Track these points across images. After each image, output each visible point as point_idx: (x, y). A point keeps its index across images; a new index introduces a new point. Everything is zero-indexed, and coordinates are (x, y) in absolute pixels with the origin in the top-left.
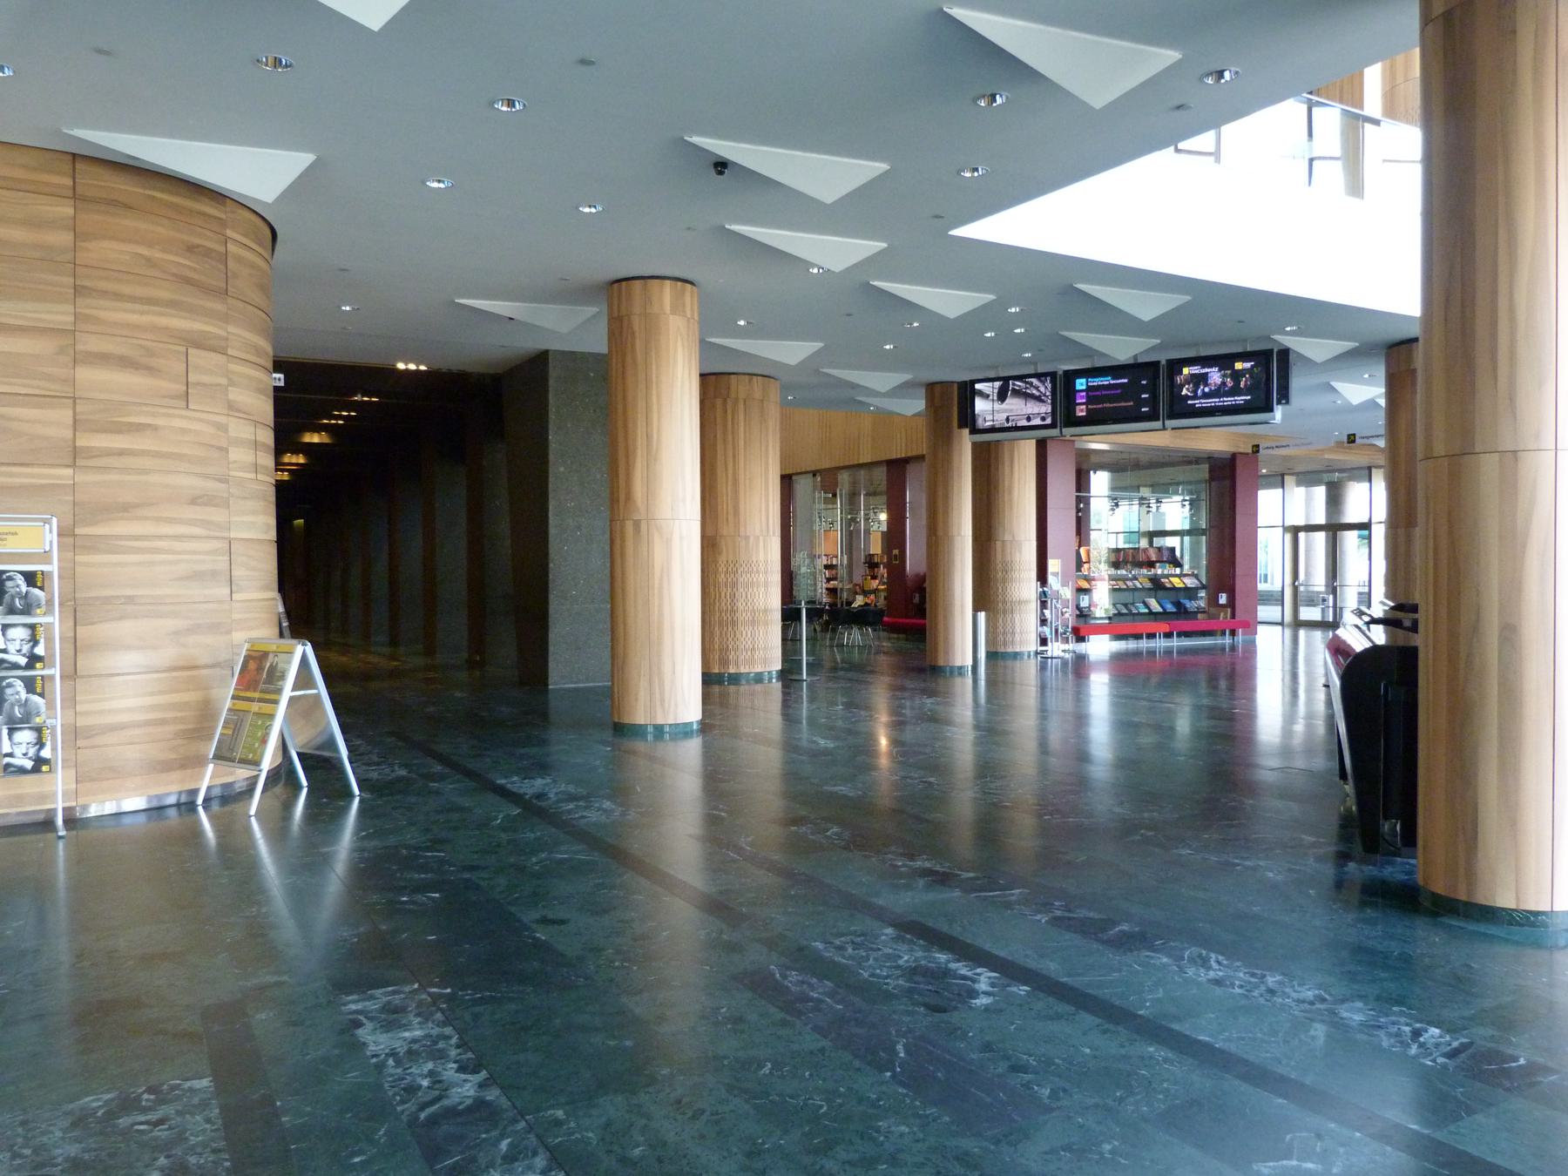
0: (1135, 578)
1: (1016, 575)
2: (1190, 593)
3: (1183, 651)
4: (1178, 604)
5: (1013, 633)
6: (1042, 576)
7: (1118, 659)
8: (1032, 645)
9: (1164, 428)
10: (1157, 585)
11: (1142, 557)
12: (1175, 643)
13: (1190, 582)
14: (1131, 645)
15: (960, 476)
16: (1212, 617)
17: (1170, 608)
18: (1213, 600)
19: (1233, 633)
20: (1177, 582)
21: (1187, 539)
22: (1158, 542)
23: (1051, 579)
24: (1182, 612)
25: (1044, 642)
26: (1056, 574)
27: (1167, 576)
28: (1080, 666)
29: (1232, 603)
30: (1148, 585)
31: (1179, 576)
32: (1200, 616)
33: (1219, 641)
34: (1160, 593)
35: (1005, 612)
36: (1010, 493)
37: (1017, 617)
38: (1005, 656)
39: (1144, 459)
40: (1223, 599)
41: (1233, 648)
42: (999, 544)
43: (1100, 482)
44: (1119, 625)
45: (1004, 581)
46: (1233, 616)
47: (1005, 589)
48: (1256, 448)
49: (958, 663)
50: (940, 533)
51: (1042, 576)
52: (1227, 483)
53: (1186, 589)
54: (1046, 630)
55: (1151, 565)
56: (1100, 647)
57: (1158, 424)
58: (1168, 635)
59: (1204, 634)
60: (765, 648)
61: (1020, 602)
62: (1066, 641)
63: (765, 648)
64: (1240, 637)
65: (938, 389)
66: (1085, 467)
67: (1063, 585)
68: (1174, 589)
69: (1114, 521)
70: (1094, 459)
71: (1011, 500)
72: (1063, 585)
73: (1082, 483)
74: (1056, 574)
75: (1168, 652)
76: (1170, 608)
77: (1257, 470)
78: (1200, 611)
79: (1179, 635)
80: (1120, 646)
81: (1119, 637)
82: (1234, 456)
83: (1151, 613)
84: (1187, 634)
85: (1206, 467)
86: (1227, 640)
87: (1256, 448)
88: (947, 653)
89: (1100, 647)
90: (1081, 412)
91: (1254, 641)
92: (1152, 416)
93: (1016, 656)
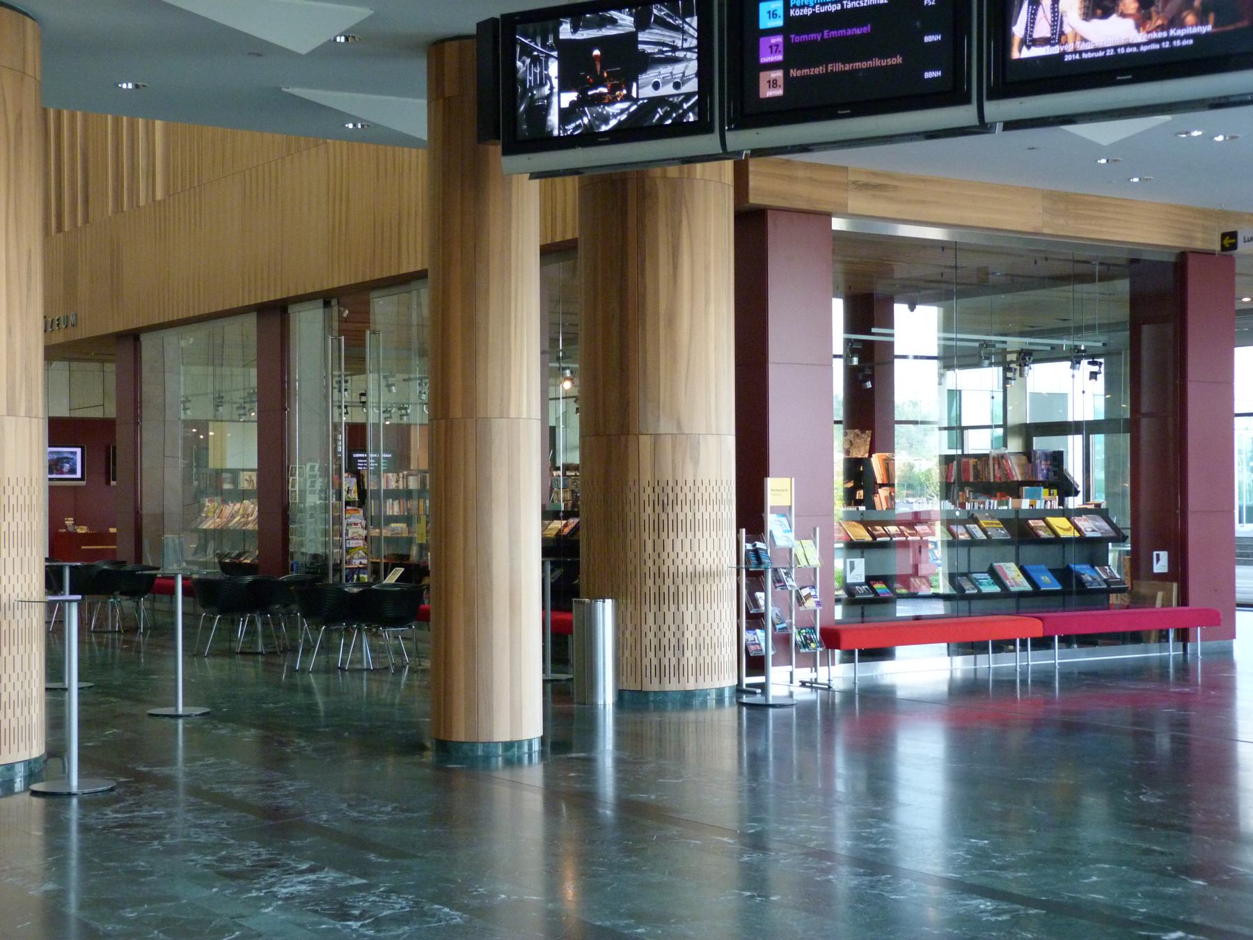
0: (973, 519)
1: (685, 513)
2: (1093, 549)
3: (1073, 678)
4: (1064, 574)
5: (680, 648)
6: (751, 514)
7: (966, 692)
8: (723, 674)
9: (983, 127)
10: (1021, 533)
11: (993, 474)
12: (1057, 658)
13: (1090, 527)
14: (987, 663)
15: (506, 271)
16: (1138, 600)
17: (1048, 582)
18: (1138, 563)
19: (1183, 636)
20: (1061, 525)
21: (1098, 441)
22: (1042, 444)
23: (774, 523)
24: (1072, 589)
25: (756, 664)
26: (784, 512)
27: (1042, 515)
28: (875, 713)
29: (1179, 571)
30: (1000, 533)
31: (1067, 513)
32: (1114, 599)
33: (1151, 653)
34: (1028, 551)
35: (660, 598)
36: (672, 321)
37: (688, 610)
38: (660, 701)
39: (999, 268)
40: (1161, 564)
41: (1184, 669)
42: (645, 441)
43: (915, 328)
44: (968, 622)
45: (658, 527)
46: (1183, 600)
47: (659, 547)
48: (1230, 239)
49: (502, 733)
50: (457, 412)
51: (751, 514)
52: (1169, 329)
53: (1083, 541)
54: (760, 639)
55: (1013, 489)
56: (922, 670)
57: (963, 115)
58: (1042, 643)
59: (1136, 638)
60: (698, 647)
61: (695, 576)
62: (810, 661)
63: (698, 647)
64: (1198, 646)
65: (451, 48)
66: (880, 288)
67: (800, 536)
68: (1057, 541)
69: (944, 399)
70: (901, 271)
71: (673, 344)
72: (800, 536)
73: (867, 312)
74: (784, 512)
75: (1043, 680)
76: (1048, 582)
77: (1231, 298)
78: (1111, 588)
79: (1066, 641)
80: (961, 666)
81: (972, 647)
82: (1183, 257)
83: (1006, 593)
84: (1087, 640)
85: (1122, 286)
86: (1172, 651)
87: (1230, 239)
88: (472, 708)
89: (922, 670)
90: (771, 86)
91: (1228, 653)
92: (951, 94)
93: (687, 699)
